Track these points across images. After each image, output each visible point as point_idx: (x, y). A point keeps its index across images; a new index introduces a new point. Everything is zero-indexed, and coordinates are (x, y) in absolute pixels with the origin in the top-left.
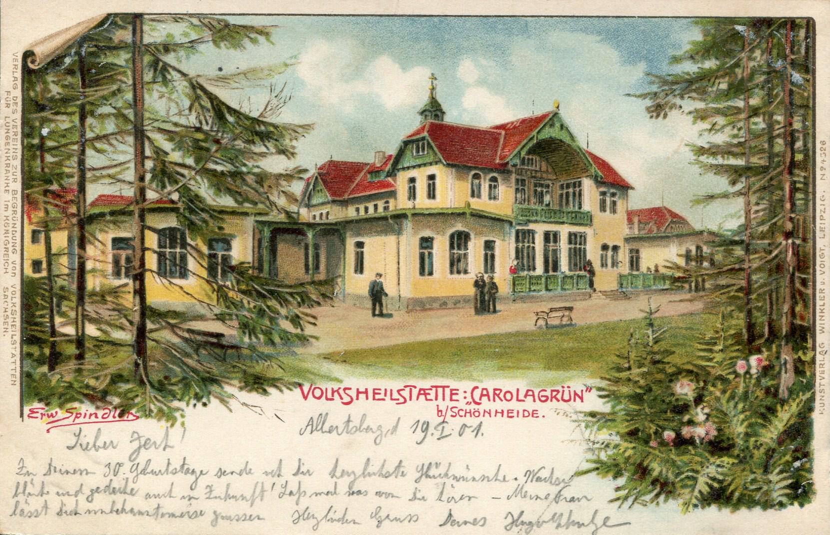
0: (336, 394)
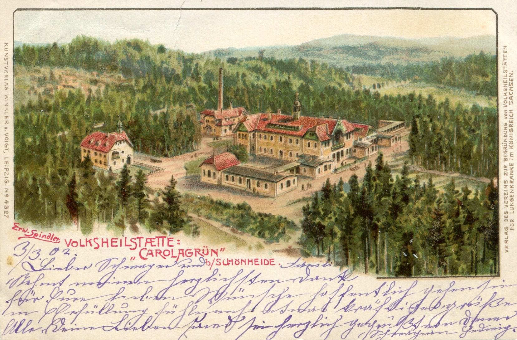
0: (88, 243)
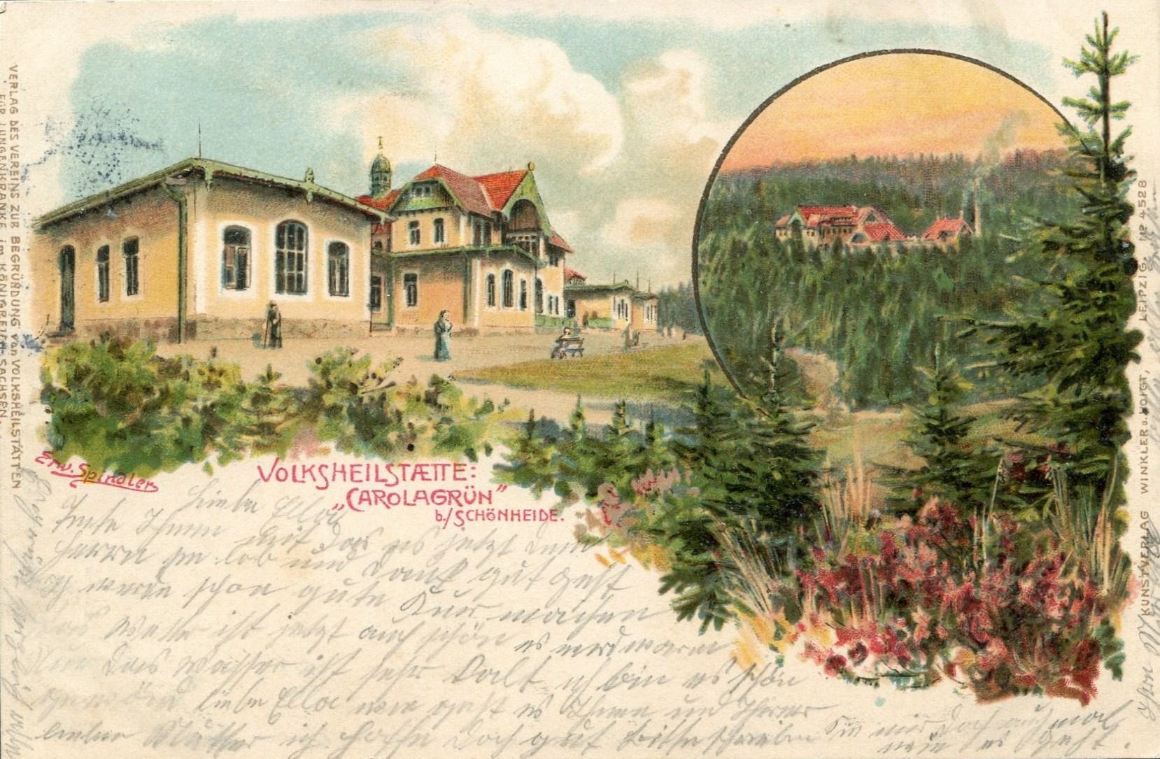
0: (308, 474)
